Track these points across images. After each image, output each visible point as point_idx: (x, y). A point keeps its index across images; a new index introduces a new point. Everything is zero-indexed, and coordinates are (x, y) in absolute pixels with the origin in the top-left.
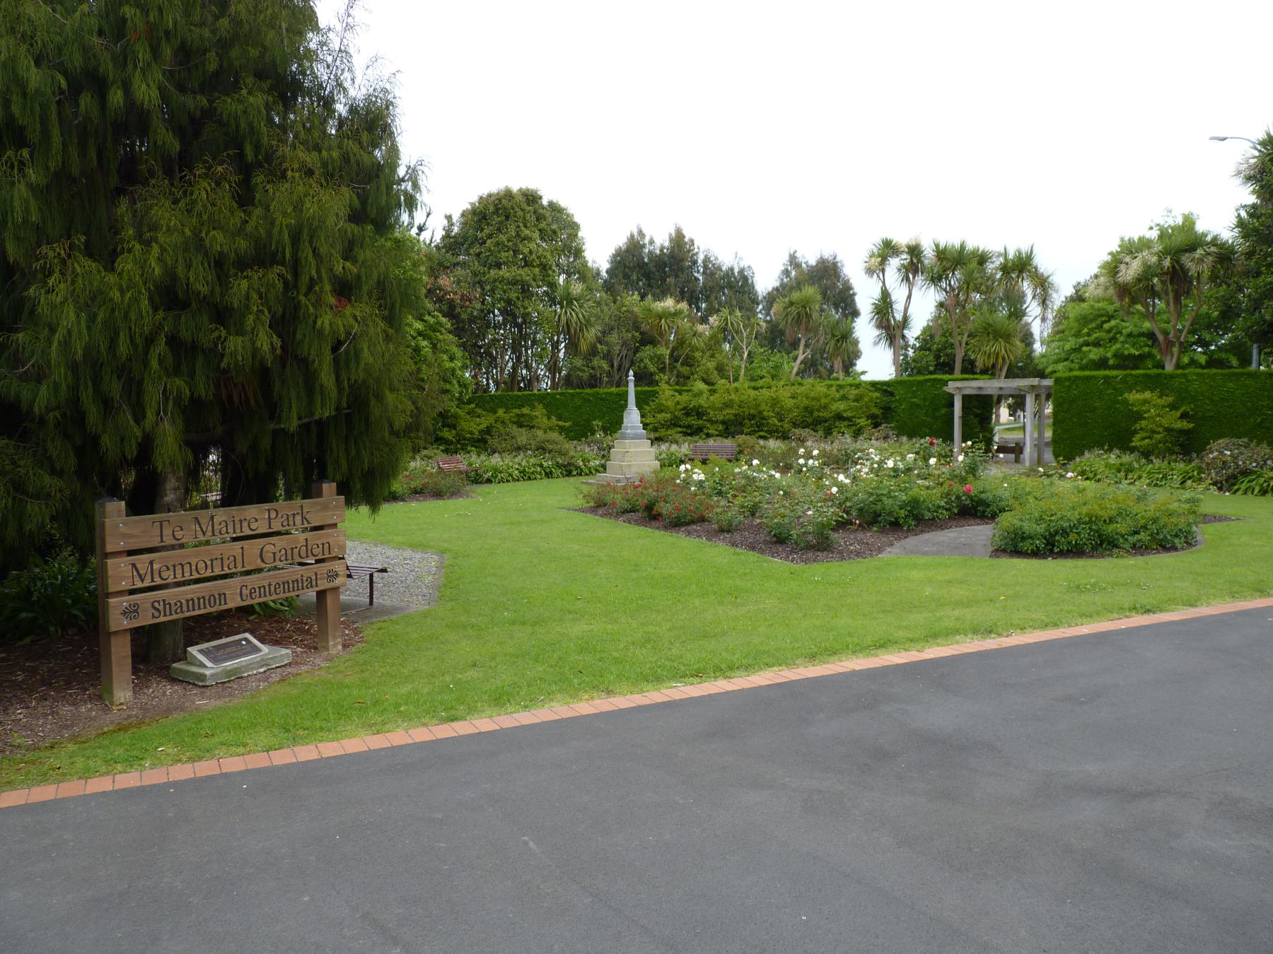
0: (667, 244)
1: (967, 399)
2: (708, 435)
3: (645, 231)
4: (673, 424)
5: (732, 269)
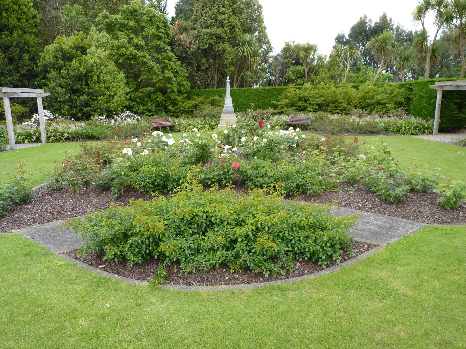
0: (378, 21)
1: (446, 94)
2: (309, 111)
3: (367, 16)
4: (292, 105)
5: (411, 32)
